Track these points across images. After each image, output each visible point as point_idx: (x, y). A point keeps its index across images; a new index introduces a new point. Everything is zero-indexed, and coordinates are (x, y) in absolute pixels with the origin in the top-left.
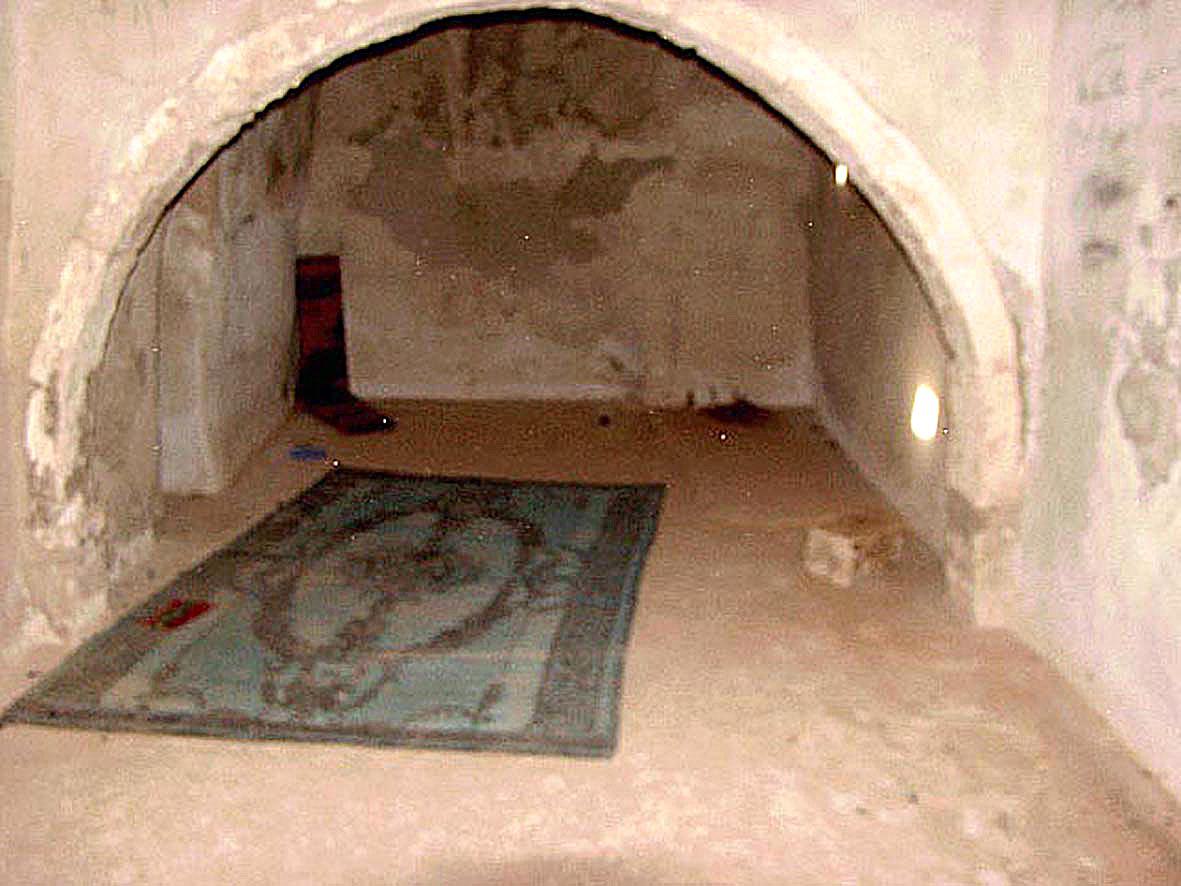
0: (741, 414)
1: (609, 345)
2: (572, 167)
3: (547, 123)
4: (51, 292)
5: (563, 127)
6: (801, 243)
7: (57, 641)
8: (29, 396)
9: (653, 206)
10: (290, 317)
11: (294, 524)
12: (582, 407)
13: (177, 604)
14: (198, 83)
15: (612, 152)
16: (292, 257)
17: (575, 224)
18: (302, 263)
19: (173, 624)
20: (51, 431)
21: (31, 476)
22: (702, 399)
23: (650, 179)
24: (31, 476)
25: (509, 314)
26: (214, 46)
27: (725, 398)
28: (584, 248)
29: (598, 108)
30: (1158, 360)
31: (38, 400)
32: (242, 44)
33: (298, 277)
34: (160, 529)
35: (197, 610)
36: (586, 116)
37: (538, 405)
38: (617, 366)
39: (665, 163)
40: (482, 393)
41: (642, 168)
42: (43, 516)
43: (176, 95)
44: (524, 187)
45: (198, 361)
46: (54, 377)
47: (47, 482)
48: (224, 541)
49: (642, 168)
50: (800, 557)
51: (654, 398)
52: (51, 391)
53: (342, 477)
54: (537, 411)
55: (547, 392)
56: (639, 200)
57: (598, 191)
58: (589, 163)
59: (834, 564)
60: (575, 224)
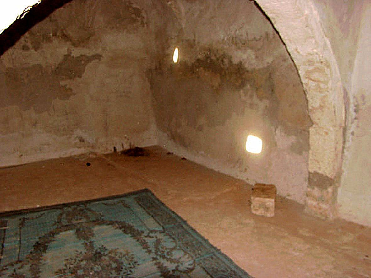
0: (135, 153)
1: (79, 132)
2: (61, 59)
3: (49, 40)
5: (55, 41)
6: (148, 85)
9: (94, 74)
12: (71, 160)
15: (76, 52)
17: (62, 83)
22: (119, 149)
23: (91, 64)
25: (35, 125)
27: (127, 147)
28: (66, 93)
29: (70, 33)
36: (66, 37)
37: (51, 161)
38: (82, 140)
39: (98, 57)
40: (26, 160)
41: (89, 59)
44: (38, 68)
48: (313, 9)
49: (89, 59)
50: (250, 209)
51: (100, 151)
55: (54, 156)
56: (88, 71)
57: (72, 68)
58: (68, 56)
59: (267, 209)
60: (62, 83)
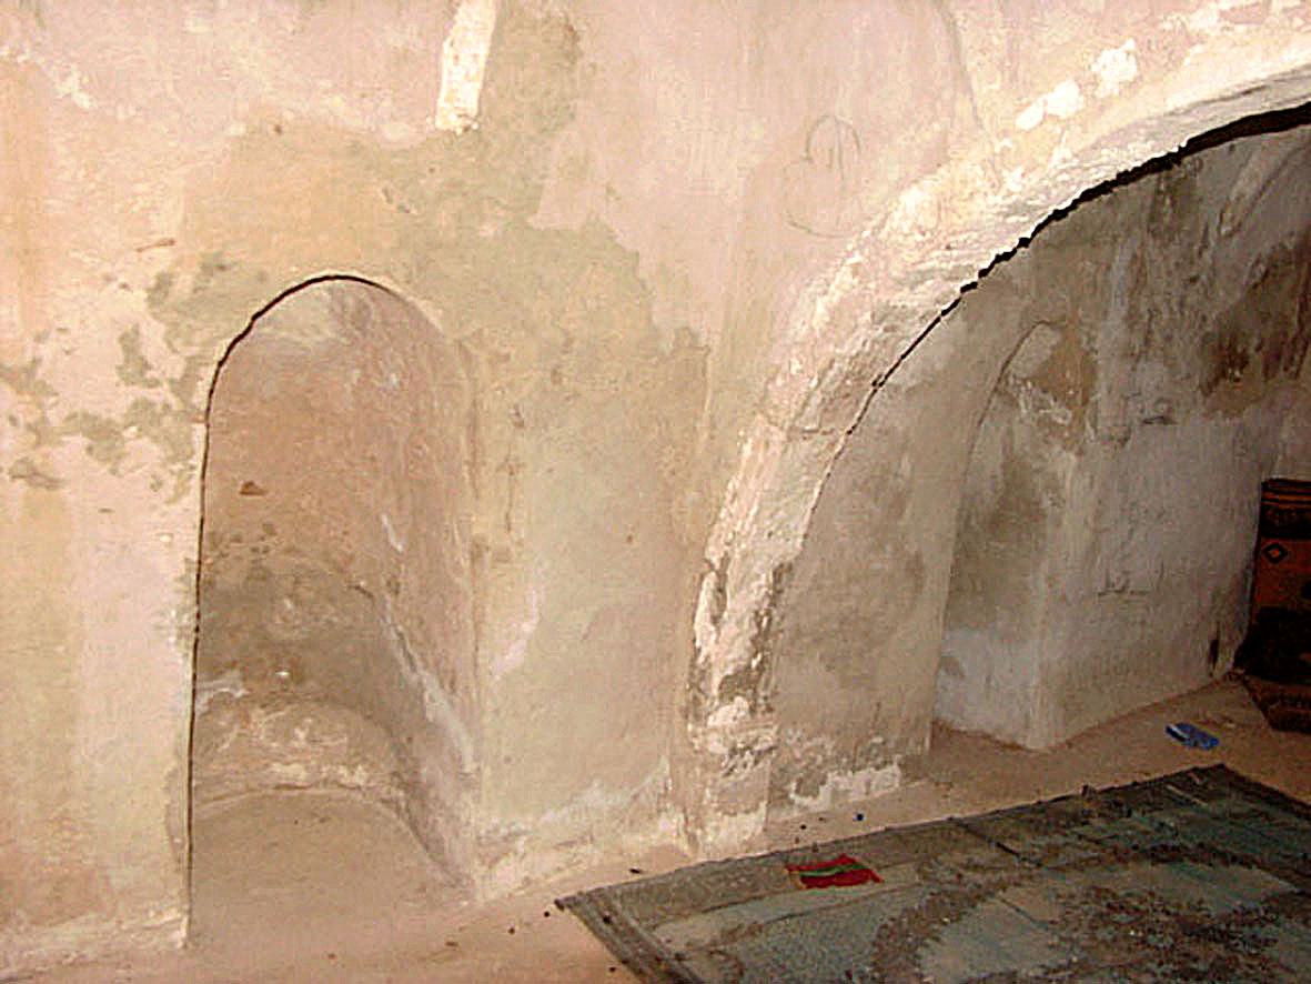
4: (732, 468)
7: (685, 847)
8: (702, 578)
10: (1244, 554)
11: (1081, 818)
13: (843, 859)
14: (883, 235)
16: (1255, 482)
18: (1269, 487)
19: (811, 882)
20: (715, 620)
21: (693, 665)
24: (693, 665)
26: (900, 187)
30: (1290, 136)
31: (710, 582)
32: (927, 182)
33: (1263, 509)
34: (911, 768)
35: (859, 875)
42: (695, 711)
43: (860, 248)
45: (1043, 586)
46: (725, 561)
47: (704, 675)
52: (722, 576)
53: (1221, 778)
54: (1070, 707)
